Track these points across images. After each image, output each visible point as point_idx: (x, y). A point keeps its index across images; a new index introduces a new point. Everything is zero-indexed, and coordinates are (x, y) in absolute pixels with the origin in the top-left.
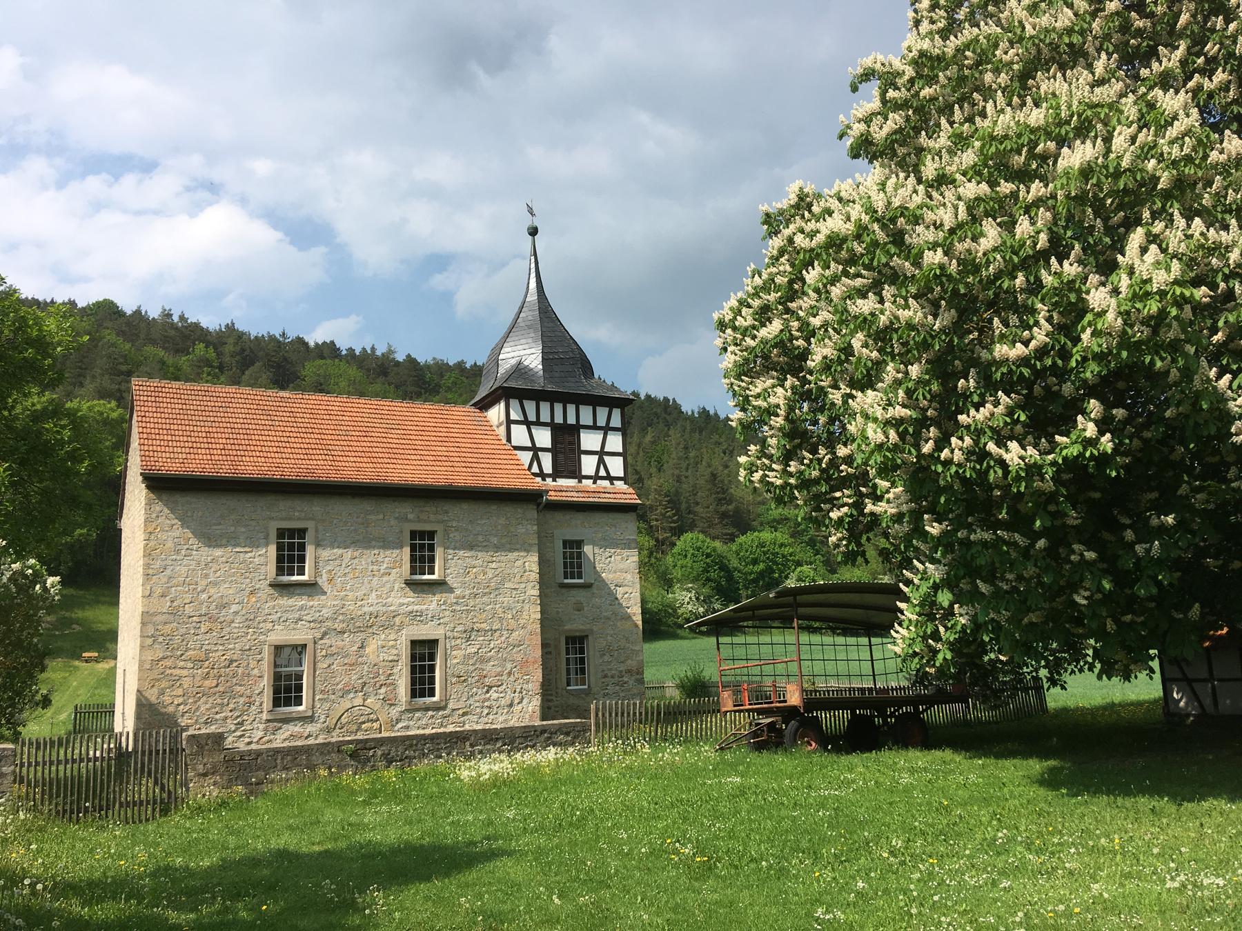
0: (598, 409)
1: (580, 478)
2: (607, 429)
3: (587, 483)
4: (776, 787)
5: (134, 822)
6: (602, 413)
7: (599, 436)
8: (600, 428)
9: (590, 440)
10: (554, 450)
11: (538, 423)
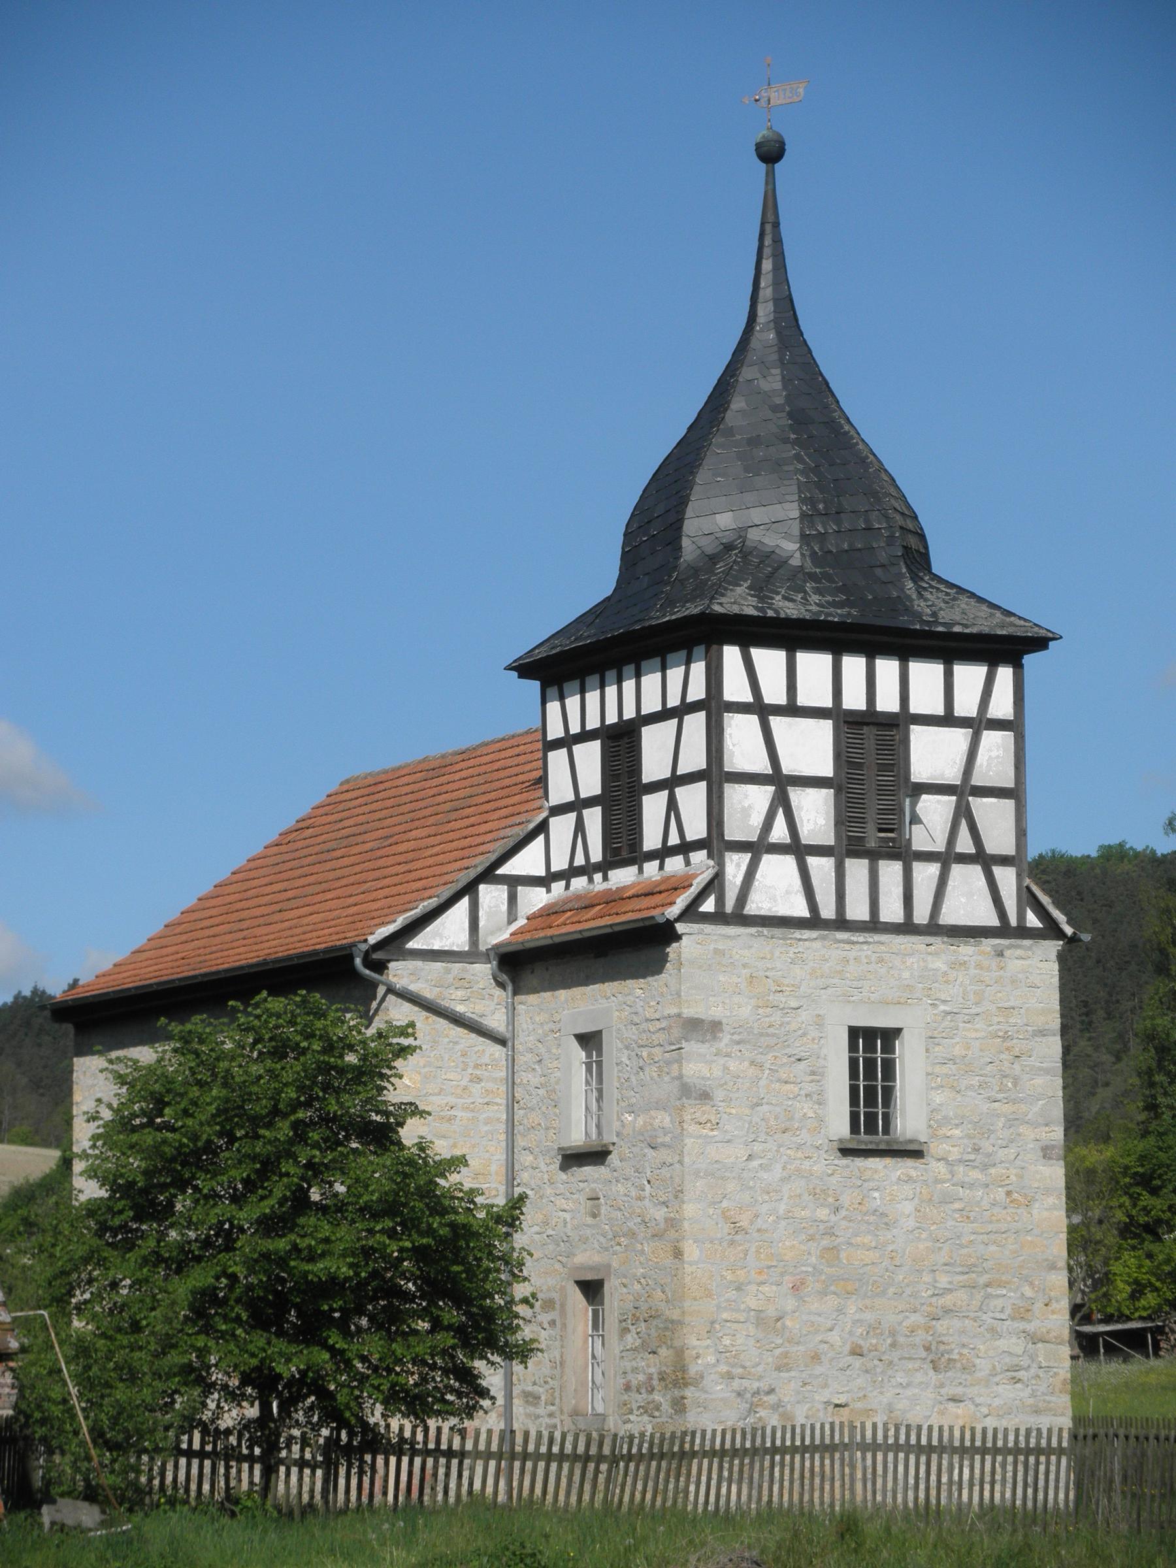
0: (803, 658)
2: (979, 724)
3: (651, 868)
4: (994, 1544)
5: (908, 1427)
6: (969, 676)
7: (959, 738)
8: (964, 722)
11: (792, 709)
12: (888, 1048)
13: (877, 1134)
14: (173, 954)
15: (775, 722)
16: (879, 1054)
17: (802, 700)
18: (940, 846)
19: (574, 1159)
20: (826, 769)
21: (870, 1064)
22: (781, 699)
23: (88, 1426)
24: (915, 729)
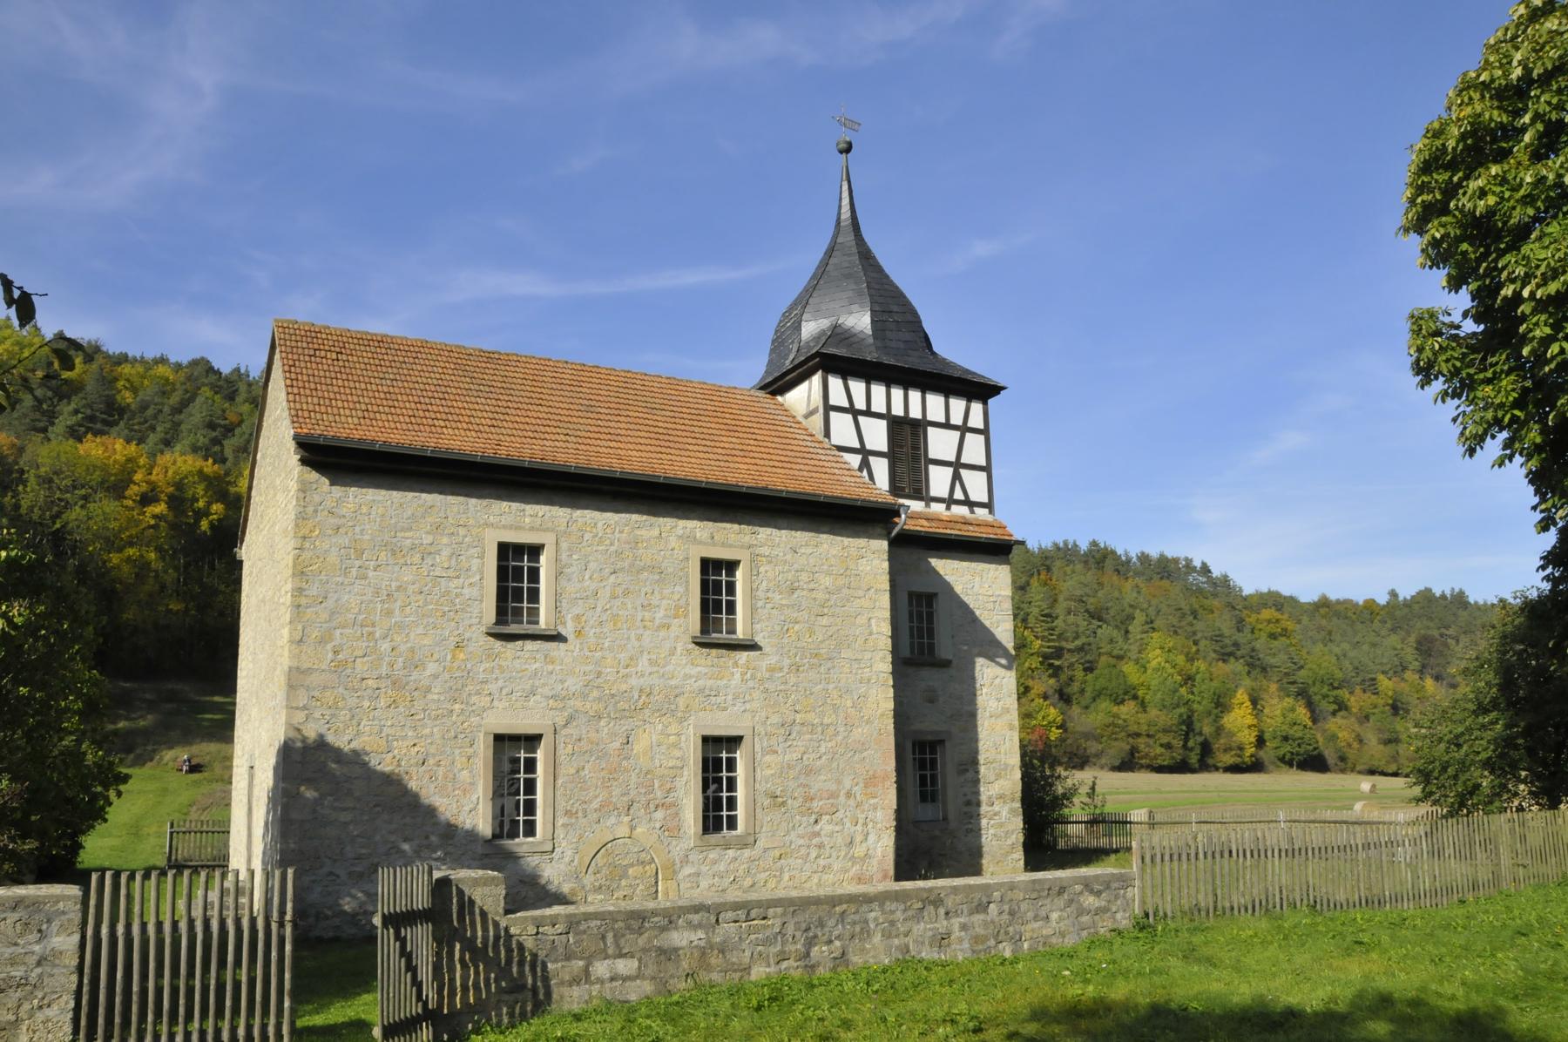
1: (930, 500)
2: (964, 429)
6: (958, 405)
8: (955, 428)
9: (940, 444)
10: (892, 455)
11: (868, 413)
12: (930, 605)
13: (722, 632)
14: (142, 915)
16: (525, 605)
17: (874, 409)
18: (945, 494)
19: (716, 815)
20: (885, 449)
21: (920, 615)
24: (930, 429)
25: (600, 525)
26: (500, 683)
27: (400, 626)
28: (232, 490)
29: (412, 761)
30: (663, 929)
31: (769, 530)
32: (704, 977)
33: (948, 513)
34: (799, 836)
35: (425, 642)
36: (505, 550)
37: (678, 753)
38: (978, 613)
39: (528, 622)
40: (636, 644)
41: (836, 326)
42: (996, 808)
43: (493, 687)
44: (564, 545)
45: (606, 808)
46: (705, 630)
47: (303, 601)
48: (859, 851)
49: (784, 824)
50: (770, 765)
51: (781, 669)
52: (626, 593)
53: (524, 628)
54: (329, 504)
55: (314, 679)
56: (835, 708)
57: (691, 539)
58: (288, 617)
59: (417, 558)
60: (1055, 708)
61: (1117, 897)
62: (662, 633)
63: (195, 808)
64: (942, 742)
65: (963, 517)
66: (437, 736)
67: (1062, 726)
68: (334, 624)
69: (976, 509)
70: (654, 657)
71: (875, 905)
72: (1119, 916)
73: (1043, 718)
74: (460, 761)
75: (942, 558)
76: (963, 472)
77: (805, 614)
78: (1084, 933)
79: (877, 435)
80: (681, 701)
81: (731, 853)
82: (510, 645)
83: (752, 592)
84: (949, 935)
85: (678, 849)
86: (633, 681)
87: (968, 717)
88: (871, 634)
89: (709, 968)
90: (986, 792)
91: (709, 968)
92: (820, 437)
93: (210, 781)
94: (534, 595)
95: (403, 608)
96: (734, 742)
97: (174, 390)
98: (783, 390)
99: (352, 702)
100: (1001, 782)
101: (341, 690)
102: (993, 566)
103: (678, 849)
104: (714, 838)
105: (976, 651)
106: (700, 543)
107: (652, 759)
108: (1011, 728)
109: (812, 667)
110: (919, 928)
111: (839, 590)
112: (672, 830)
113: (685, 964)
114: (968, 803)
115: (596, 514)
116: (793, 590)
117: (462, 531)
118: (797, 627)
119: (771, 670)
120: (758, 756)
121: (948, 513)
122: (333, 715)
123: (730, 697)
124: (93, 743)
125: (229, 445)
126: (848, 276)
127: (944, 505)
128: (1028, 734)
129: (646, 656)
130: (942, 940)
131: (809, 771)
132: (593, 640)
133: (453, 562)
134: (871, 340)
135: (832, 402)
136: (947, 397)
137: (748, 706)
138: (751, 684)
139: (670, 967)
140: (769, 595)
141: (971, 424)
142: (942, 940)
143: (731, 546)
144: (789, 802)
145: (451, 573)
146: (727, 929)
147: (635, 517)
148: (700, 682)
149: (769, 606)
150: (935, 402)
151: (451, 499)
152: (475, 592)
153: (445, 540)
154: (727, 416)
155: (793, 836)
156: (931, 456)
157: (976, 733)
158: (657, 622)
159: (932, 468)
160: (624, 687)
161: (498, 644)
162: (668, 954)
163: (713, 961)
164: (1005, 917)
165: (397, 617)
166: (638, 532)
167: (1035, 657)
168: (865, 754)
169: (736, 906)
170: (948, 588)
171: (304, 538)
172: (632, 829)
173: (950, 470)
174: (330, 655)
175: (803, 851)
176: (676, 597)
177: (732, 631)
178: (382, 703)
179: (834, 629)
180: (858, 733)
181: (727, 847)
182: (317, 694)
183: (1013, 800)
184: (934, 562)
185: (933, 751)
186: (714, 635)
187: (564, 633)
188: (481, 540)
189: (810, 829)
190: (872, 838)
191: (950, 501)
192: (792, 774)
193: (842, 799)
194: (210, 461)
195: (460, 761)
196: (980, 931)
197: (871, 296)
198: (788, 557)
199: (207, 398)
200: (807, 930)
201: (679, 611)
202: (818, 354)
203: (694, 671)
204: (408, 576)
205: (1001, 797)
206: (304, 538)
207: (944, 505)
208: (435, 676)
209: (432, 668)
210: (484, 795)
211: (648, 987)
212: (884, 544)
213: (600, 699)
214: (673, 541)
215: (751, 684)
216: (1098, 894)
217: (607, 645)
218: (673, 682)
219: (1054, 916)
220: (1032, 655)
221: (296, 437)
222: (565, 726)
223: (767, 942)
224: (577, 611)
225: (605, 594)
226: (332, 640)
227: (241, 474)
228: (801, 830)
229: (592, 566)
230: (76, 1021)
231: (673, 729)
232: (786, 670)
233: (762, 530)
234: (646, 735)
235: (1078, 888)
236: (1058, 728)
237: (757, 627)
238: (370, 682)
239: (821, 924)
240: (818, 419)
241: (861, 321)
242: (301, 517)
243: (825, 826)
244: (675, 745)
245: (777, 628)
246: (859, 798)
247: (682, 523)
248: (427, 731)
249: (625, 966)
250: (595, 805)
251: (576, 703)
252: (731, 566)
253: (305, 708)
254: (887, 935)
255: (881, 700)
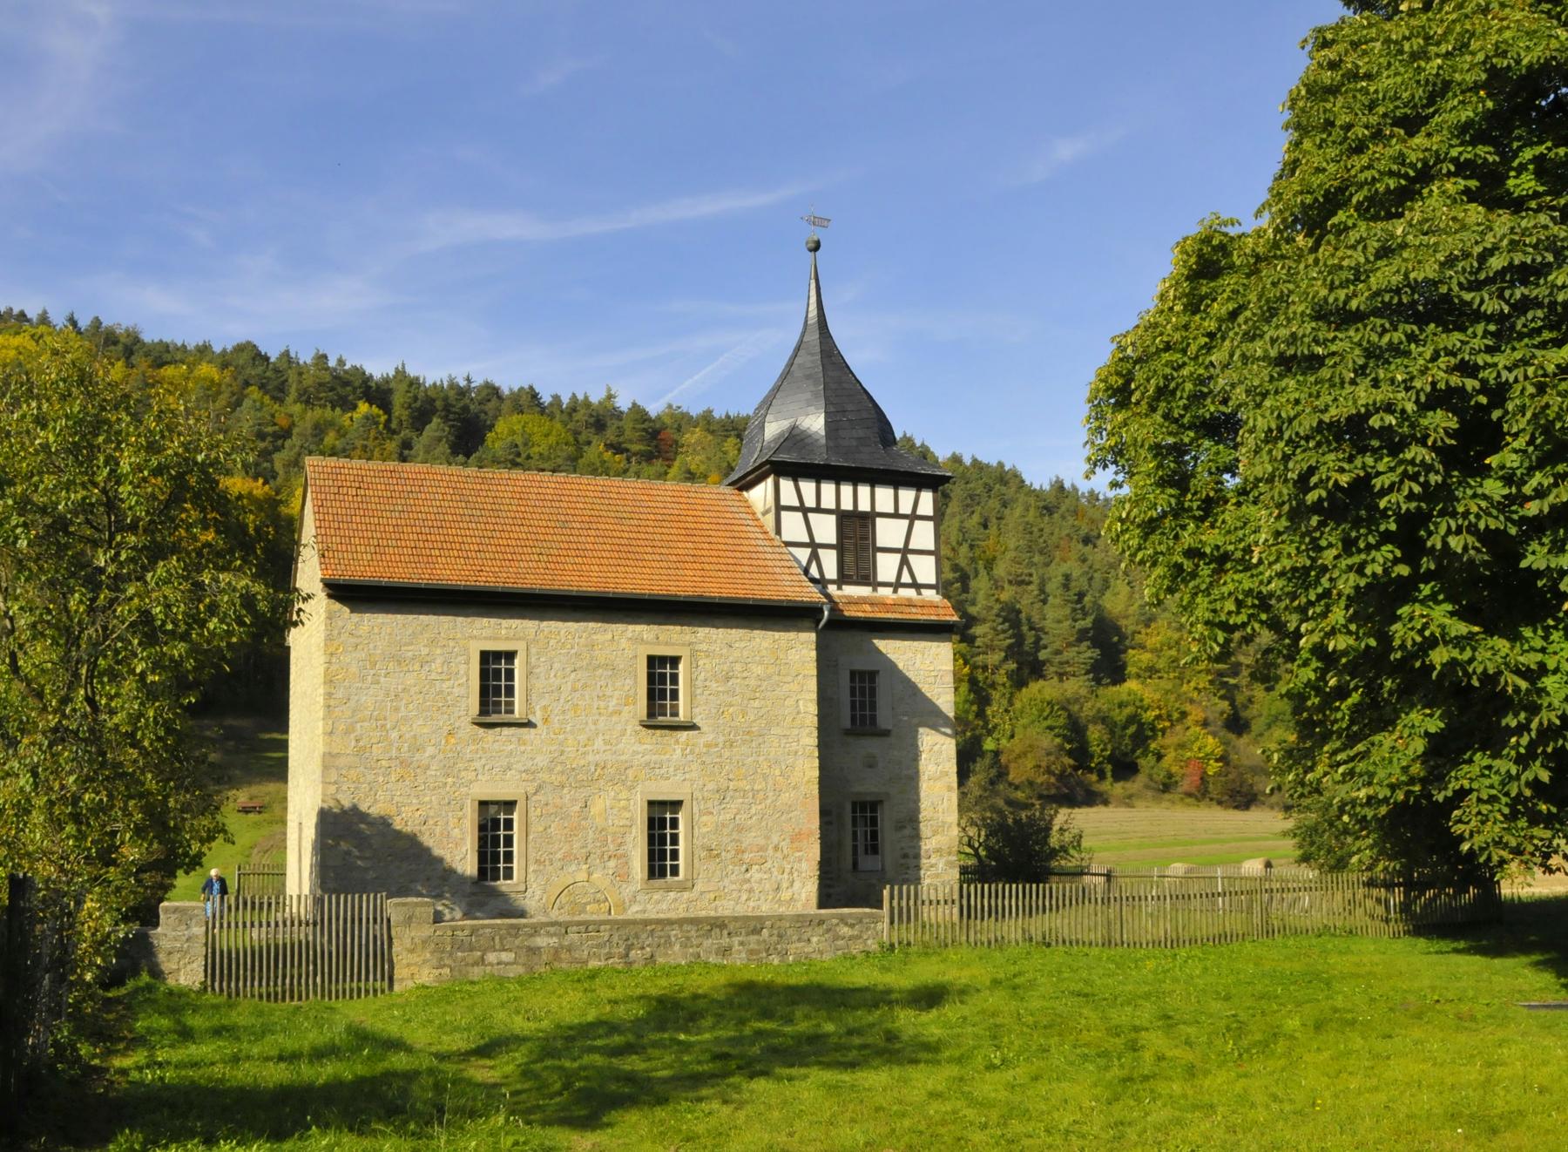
1: (876, 585)
2: (913, 517)
9: (888, 533)
10: (840, 547)
11: (818, 509)
15: (811, 516)
16: (503, 699)
17: (824, 505)
18: (892, 579)
19: (660, 860)
22: (813, 505)
23: (272, 813)
24: (879, 521)
25: (562, 632)
26: (483, 762)
27: (406, 719)
28: (283, 510)
29: (417, 822)
30: (531, 935)
31: (707, 630)
32: (556, 965)
33: (895, 596)
34: (731, 882)
35: (425, 731)
36: (485, 656)
37: (628, 815)
38: (920, 686)
39: (506, 712)
40: (593, 727)
41: (794, 427)
42: (933, 861)
43: (477, 765)
44: (533, 650)
45: (568, 858)
46: (651, 714)
47: (332, 703)
48: (785, 895)
49: (718, 872)
50: (706, 824)
51: (717, 745)
52: (585, 686)
53: (504, 717)
54: (350, 627)
55: (341, 761)
56: (765, 777)
57: (640, 640)
58: (321, 714)
59: (417, 667)
60: (1214, 738)
61: (868, 929)
62: (614, 719)
63: (256, 851)
64: (881, 802)
65: (909, 600)
66: (435, 802)
67: (1223, 759)
68: (356, 719)
69: (924, 591)
70: (607, 737)
71: (676, 926)
72: (869, 942)
73: (1200, 749)
74: (452, 822)
75: (884, 639)
76: (911, 557)
77: (738, 699)
78: (840, 952)
79: (826, 528)
80: (630, 773)
81: (672, 895)
82: (491, 731)
83: (692, 682)
84: (731, 948)
85: (628, 890)
86: (590, 758)
87: (910, 780)
88: (798, 713)
89: (560, 960)
90: (927, 845)
91: (560, 960)
92: (772, 534)
93: (270, 823)
94: (510, 691)
95: (407, 705)
96: (676, 805)
97: (219, 393)
98: (748, 486)
99: (370, 778)
100: (938, 837)
101: (362, 769)
102: (935, 644)
103: (628, 890)
104: (658, 882)
105: (916, 721)
106: (647, 643)
107: (606, 820)
108: (950, 789)
109: (744, 741)
110: (707, 943)
111: (769, 677)
112: (622, 876)
113: (544, 957)
114: (905, 856)
115: (560, 624)
116: (728, 679)
117: (452, 644)
118: (731, 710)
119: (708, 746)
120: (696, 817)
121: (895, 596)
122: (356, 788)
123: (672, 769)
124: (513, 1113)
125: (279, 459)
126: (808, 377)
127: (891, 589)
128: (1181, 767)
129: (601, 737)
130: (725, 951)
131: (740, 829)
132: (557, 726)
133: (445, 668)
134: (823, 441)
135: (783, 502)
136: (896, 489)
137: (687, 776)
138: (690, 758)
139: (536, 958)
140: (707, 683)
141: (920, 512)
142: (725, 951)
143: (673, 644)
144: (723, 854)
145: (444, 676)
146: (573, 937)
147: (591, 625)
148: (647, 757)
149: (706, 693)
150: (885, 497)
151: (443, 618)
152: (463, 691)
153: (439, 651)
154: (689, 519)
155: (726, 882)
156: (879, 544)
157: (918, 794)
158: (611, 709)
159: (880, 556)
160: (582, 762)
161: (481, 731)
162: (534, 951)
163: (563, 956)
164: (775, 938)
165: (403, 713)
166: (594, 637)
167: (1203, 675)
168: (792, 815)
169: (579, 924)
170: (892, 666)
171: (332, 654)
172: (590, 874)
173: (898, 557)
174: (353, 743)
175: (735, 894)
176: (627, 688)
177: (674, 714)
178: (393, 778)
179: (764, 710)
180: (785, 797)
181: (669, 890)
182: (344, 772)
183: (950, 854)
184: (875, 641)
185: (874, 810)
186: (660, 718)
187: (534, 720)
188: (466, 649)
189: (741, 877)
190: (797, 885)
191: (897, 585)
192: (726, 831)
193: (770, 852)
194: (261, 481)
195: (452, 822)
196: (752, 946)
197: (826, 398)
198: (725, 651)
199: (254, 401)
200: (627, 939)
201: (629, 700)
202: (768, 462)
203: (641, 748)
204: (410, 680)
205: (938, 850)
206: (332, 654)
207: (891, 589)
208: (433, 757)
209: (430, 750)
210: (472, 848)
211: (520, 970)
212: (813, 636)
213: (562, 773)
214: (624, 643)
215: (690, 758)
216: (852, 926)
217: (568, 729)
218: (623, 758)
219: (814, 939)
220: (1200, 672)
221: (322, 580)
222: (535, 794)
223: (599, 946)
224: (544, 702)
225: (567, 688)
226: (354, 731)
227: (291, 494)
228: (733, 877)
229: (556, 666)
230: (206, 971)
231: (623, 795)
232: (721, 745)
233: (700, 629)
234: (601, 801)
235: (835, 921)
236: (1217, 760)
237: (696, 711)
238: (383, 762)
239: (637, 936)
240: (771, 517)
241: (815, 423)
242: (329, 639)
243: (755, 874)
244: (625, 808)
245: (714, 711)
246: (785, 852)
247: (631, 627)
248: (427, 799)
249: (506, 956)
250: (559, 856)
251: (544, 776)
252: (675, 661)
253: (335, 783)
254: (684, 946)
255: (808, 770)
